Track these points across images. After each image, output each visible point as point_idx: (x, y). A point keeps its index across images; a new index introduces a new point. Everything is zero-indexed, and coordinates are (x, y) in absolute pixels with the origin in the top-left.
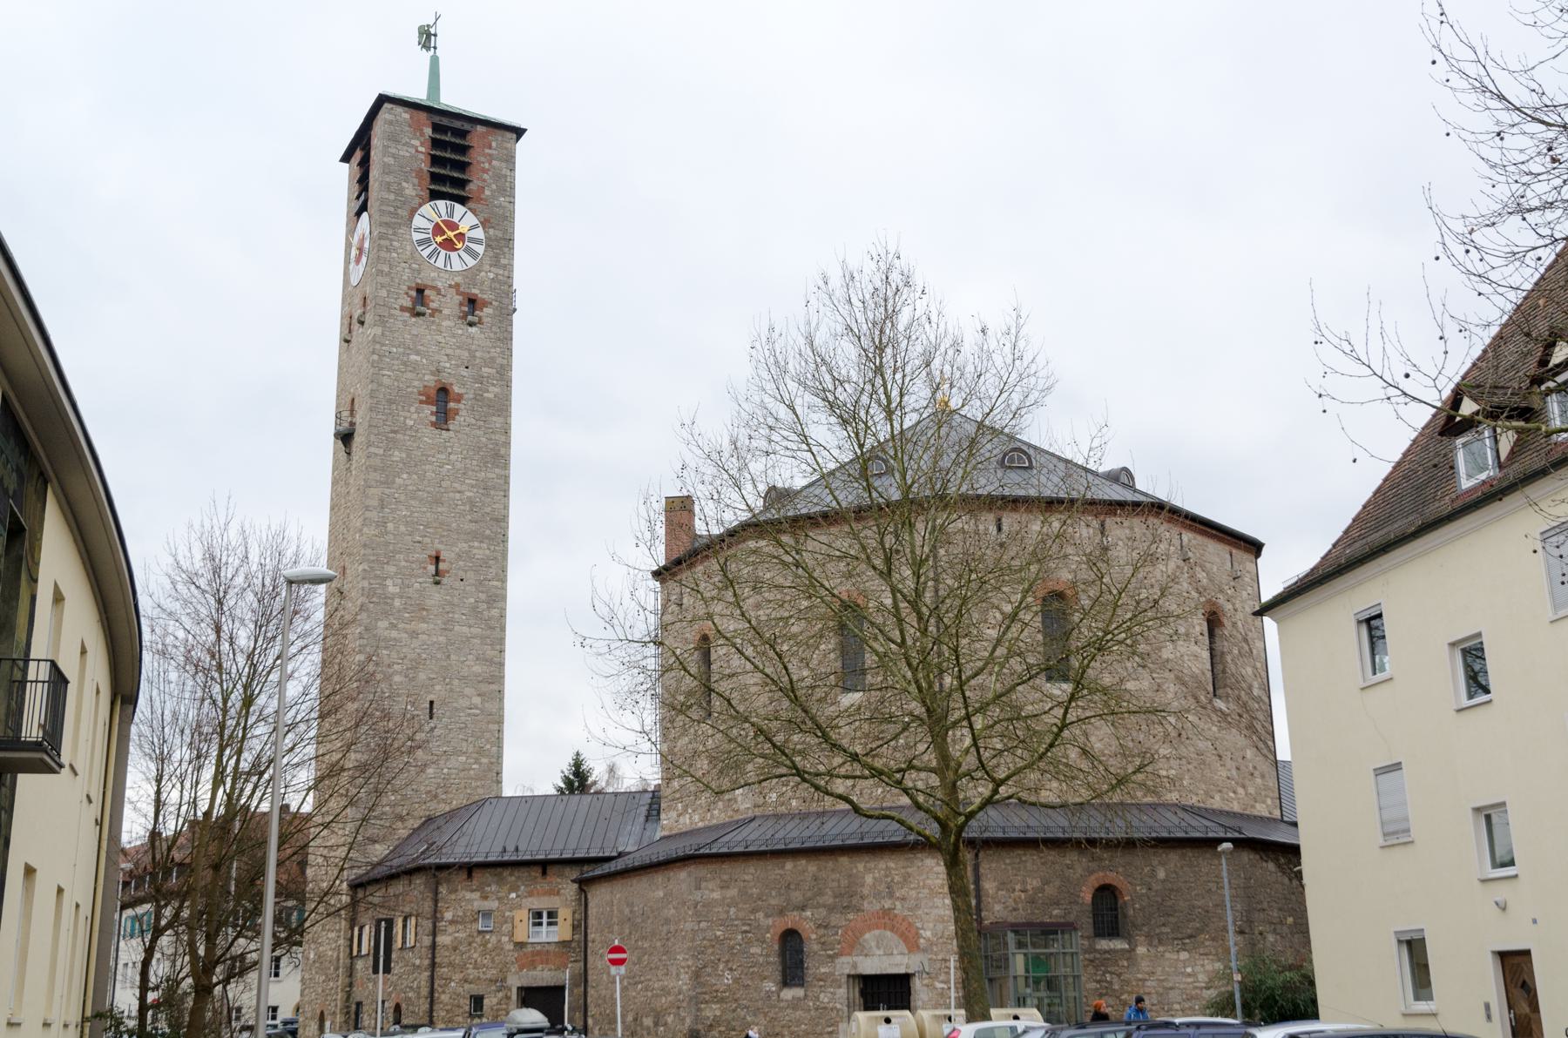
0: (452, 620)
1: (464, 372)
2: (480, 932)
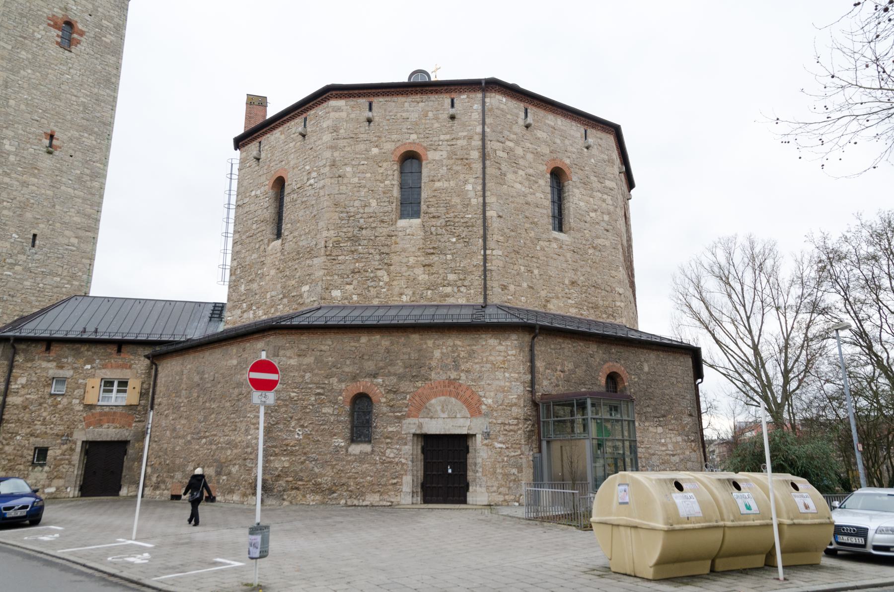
0: (60, 182)
1: (88, 18)
2: (51, 395)
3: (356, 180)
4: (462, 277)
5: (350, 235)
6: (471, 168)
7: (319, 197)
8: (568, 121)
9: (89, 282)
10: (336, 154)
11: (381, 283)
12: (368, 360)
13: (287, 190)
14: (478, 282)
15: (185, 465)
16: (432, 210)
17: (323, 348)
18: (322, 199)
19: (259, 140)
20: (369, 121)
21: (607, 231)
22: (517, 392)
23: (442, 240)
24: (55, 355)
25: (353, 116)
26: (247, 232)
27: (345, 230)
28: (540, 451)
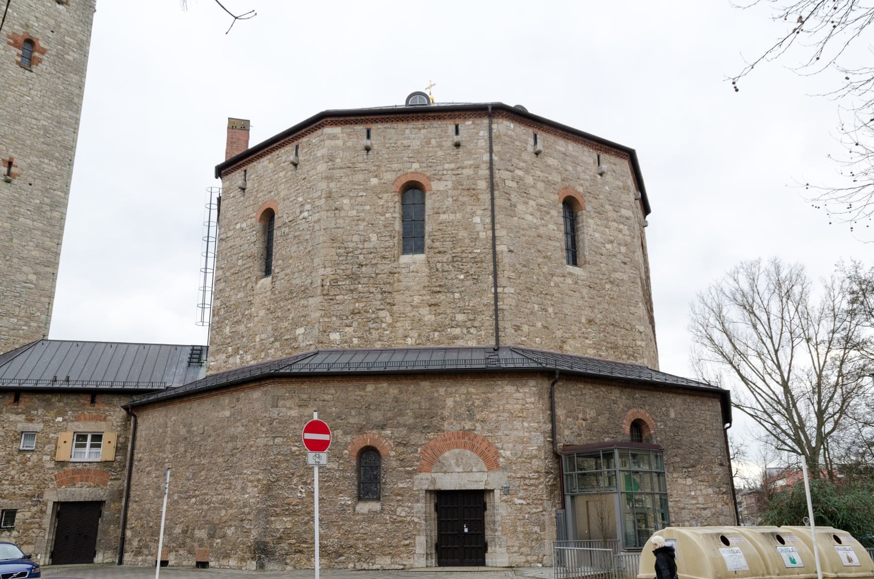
0: (18, 213)
1: (50, 35)
2: (20, 451)
3: (354, 213)
4: (471, 317)
5: (349, 272)
6: (478, 199)
7: (313, 231)
8: (580, 146)
9: (47, 323)
10: (332, 185)
11: (384, 325)
12: (375, 410)
13: (277, 223)
14: (489, 323)
15: (171, 528)
16: (437, 244)
17: (326, 397)
18: (317, 234)
19: (244, 168)
20: (368, 149)
21: (625, 263)
22: (537, 443)
23: (449, 277)
24: (24, 407)
25: (349, 144)
26: (231, 268)
27: (343, 267)
28: (564, 507)
